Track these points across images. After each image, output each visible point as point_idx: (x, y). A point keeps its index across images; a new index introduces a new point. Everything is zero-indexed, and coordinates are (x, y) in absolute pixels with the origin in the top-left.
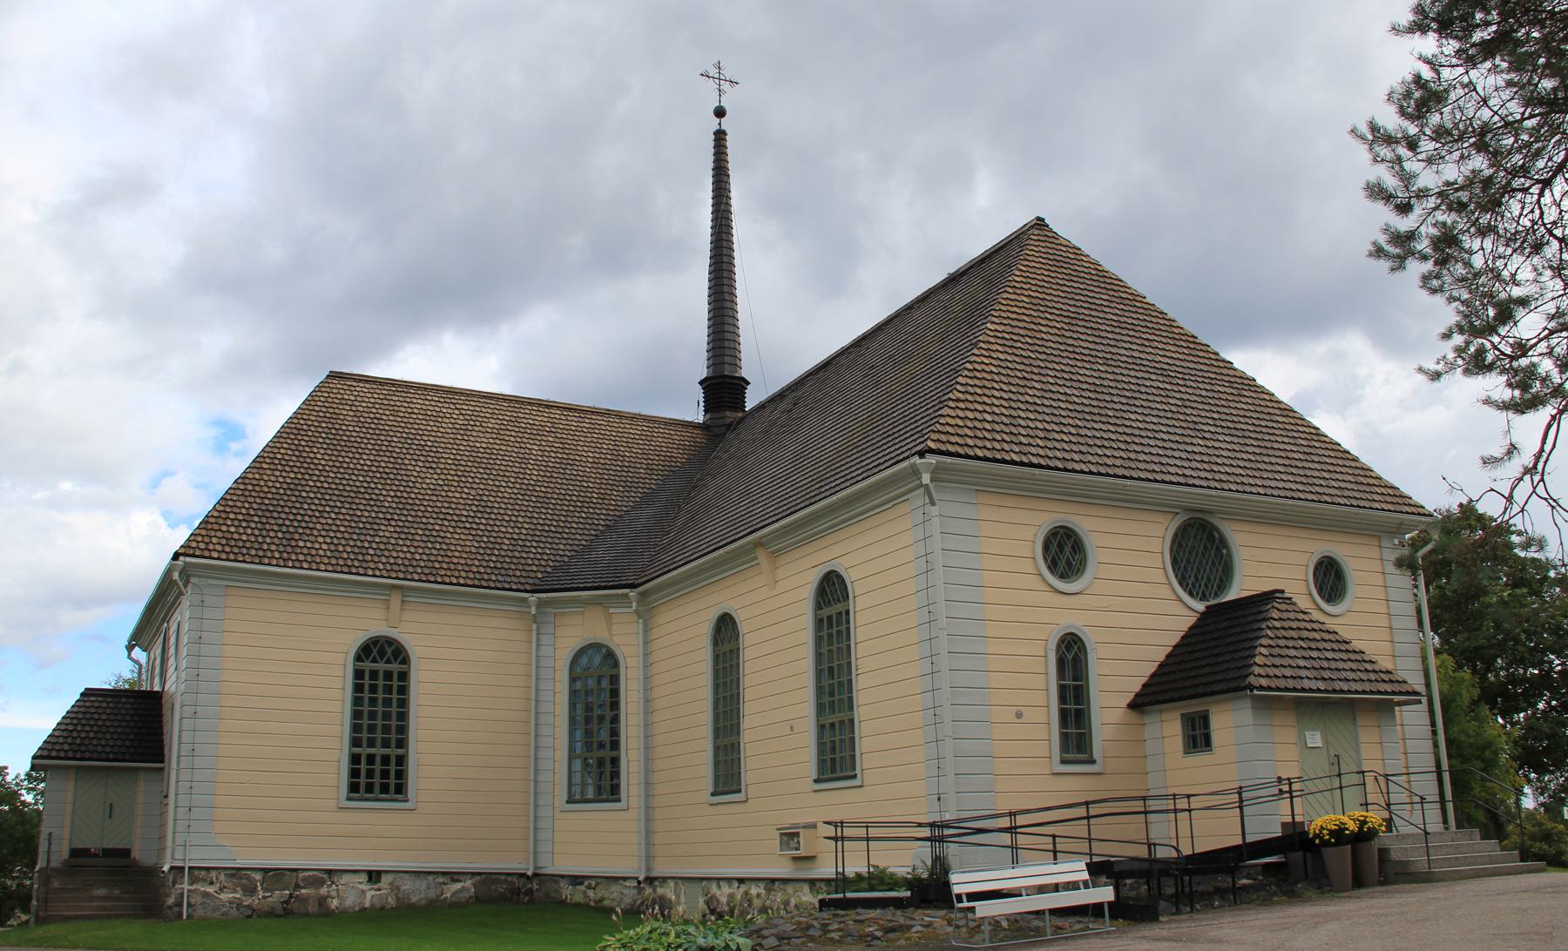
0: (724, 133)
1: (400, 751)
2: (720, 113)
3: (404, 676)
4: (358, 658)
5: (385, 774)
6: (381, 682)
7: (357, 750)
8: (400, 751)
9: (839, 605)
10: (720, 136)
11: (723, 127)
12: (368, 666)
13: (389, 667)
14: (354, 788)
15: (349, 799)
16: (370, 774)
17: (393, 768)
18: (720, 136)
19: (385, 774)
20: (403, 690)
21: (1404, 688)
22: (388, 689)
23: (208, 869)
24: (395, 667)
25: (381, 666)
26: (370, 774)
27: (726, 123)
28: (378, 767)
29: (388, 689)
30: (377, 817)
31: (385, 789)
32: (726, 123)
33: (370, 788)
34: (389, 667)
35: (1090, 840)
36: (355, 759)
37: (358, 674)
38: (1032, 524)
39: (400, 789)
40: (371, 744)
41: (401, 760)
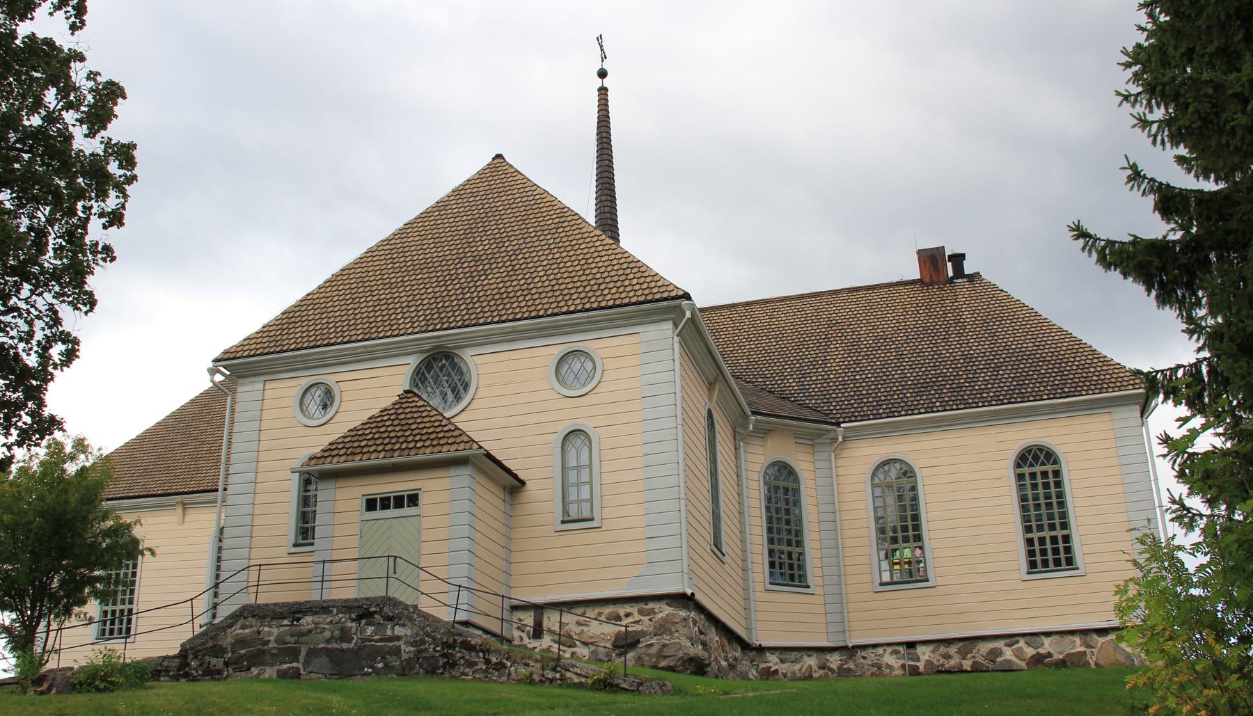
0: (606, 89)
1: (1065, 532)
2: (602, 74)
3: (1057, 473)
4: (1018, 466)
5: (1056, 551)
6: (1039, 481)
7: (1030, 535)
8: (1065, 532)
9: (224, 444)
10: (603, 91)
11: (605, 85)
12: (1026, 470)
13: (1044, 468)
14: (1033, 565)
15: (1029, 573)
16: (1043, 552)
17: (1061, 545)
18: (603, 91)
19: (1056, 551)
20: (1058, 484)
21: (687, 450)
22: (1046, 486)
23: (875, 646)
24: (1049, 468)
25: (1038, 469)
26: (1043, 552)
27: (607, 82)
28: (1049, 546)
29: (1046, 486)
30: (1054, 584)
31: (1057, 562)
32: (607, 82)
33: (1045, 563)
34: (1044, 468)
35: (456, 608)
36: (1030, 542)
37: (1020, 477)
38: (548, 352)
39: (1070, 561)
40: (1040, 528)
41: (1066, 539)
